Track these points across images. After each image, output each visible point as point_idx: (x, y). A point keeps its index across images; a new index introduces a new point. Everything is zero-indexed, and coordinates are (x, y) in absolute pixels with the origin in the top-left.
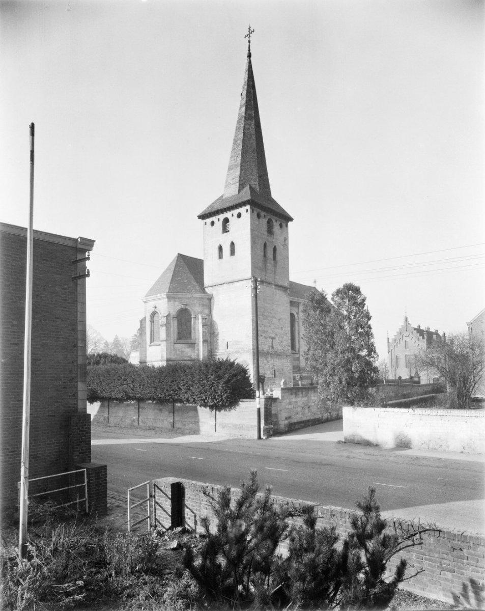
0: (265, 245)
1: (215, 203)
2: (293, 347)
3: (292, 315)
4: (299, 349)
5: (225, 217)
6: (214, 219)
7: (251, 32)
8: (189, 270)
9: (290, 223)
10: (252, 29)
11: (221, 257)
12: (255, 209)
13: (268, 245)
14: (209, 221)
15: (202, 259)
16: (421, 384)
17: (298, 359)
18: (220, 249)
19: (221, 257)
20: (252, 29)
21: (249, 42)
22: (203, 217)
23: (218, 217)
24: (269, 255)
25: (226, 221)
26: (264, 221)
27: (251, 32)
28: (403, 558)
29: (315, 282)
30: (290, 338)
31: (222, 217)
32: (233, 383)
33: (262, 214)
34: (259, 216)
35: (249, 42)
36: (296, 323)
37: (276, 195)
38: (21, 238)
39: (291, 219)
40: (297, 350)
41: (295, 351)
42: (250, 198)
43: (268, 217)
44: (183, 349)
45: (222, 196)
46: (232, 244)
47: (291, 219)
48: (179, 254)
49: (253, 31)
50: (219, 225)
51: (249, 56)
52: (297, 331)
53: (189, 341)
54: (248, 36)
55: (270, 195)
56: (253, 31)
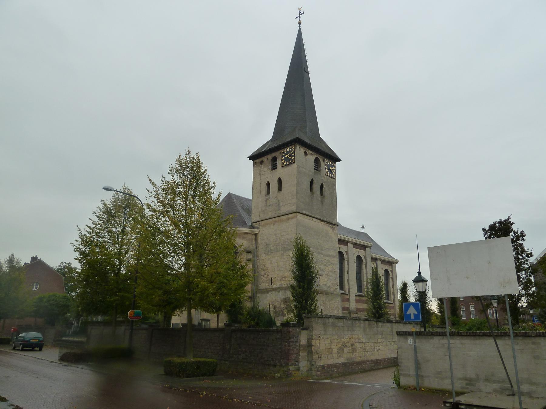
0: (312, 182)
2: (342, 287)
3: (341, 254)
7: (300, 14)
17: (348, 300)
19: (268, 192)
21: (300, 23)
23: (266, 157)
25: (275, 159)
27: (300, 14)
28: (512, 220)
29: (363, 227)
30: (338, 276)
31: (270, 157)
33: (309, 152)
35: (300, 23)
36: (346, 262)
38: (100, 318)
39: (338, 160)
41: (345, 291)
43: (316, 156)
47: (338, 160)
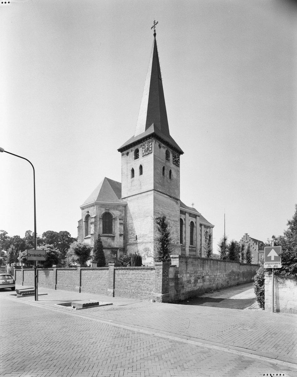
0: (164, 168)
1: (130, 140)
2: (181, 242)
3: (181, 220)
4: (185, 243)
5: (136, 148)
6: (129, 150)
7: (155, 23)
8: (112, 186)
9: (181, 156)
10: (156, 22)
11: (133, 175)
12: (157, 141)
13: (166, 168)
14: (125, 152)
15: (120, 182)
16: (172, 265)
18: (133, 171)
19: (133, 175)
20: (156, 22)
22: (121, 150)
24: (167, 181)
25: (137, 151)
26: (163, 151)
27: (155, 23)
29: (193, 204)
31: (134, 149)
32: (285, 262)
33: (163, 145)
34: (160, 147)
37: (172, 133)
40: (184, 243)
41: (183, 244)
42: (154, 131)
44: (107, 240)
45: (134, 136)
46: (141, 167)
47: (182, 153)
48: (106, 178)
49: (157, 23)
50: (132, 154)
51: (155, 35)
52: (184, 232)
53: (112, 235)
54: (155, 23)
55: (169, 134)
56: (157, 23)
